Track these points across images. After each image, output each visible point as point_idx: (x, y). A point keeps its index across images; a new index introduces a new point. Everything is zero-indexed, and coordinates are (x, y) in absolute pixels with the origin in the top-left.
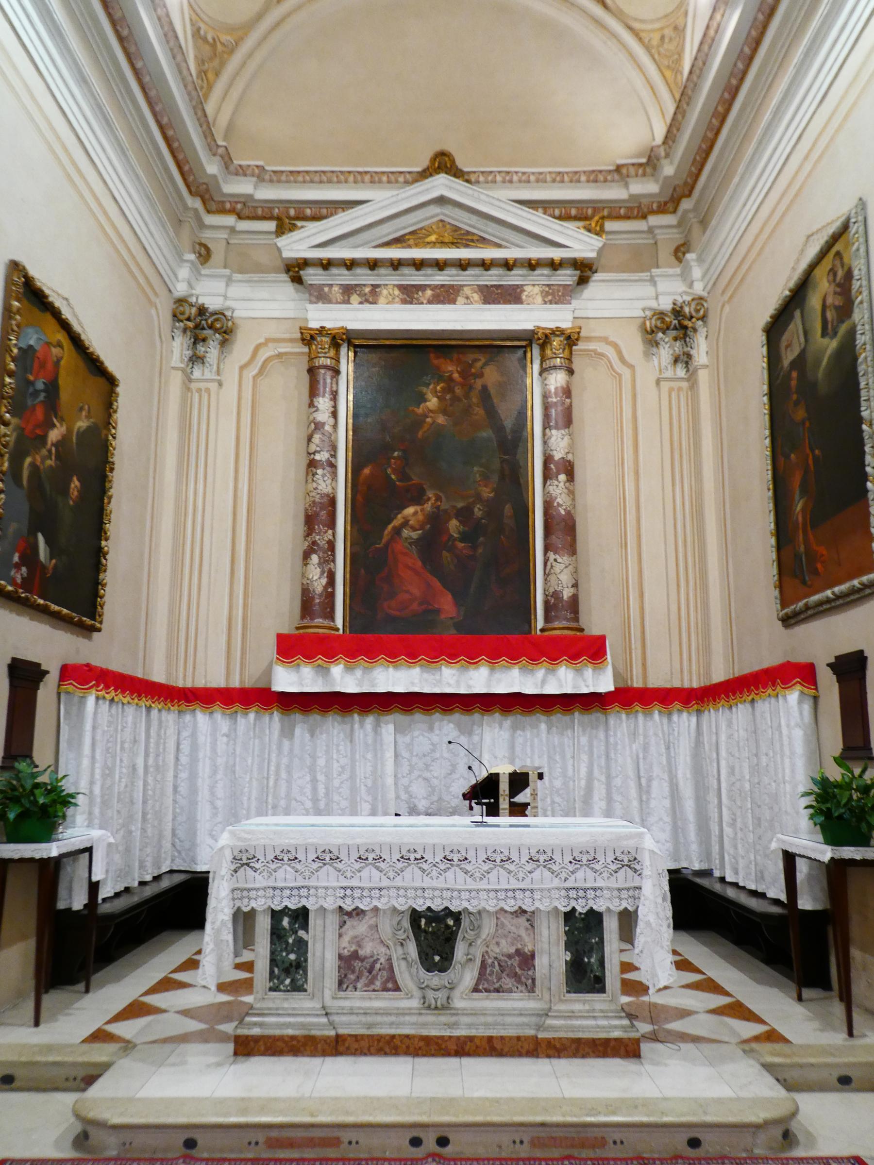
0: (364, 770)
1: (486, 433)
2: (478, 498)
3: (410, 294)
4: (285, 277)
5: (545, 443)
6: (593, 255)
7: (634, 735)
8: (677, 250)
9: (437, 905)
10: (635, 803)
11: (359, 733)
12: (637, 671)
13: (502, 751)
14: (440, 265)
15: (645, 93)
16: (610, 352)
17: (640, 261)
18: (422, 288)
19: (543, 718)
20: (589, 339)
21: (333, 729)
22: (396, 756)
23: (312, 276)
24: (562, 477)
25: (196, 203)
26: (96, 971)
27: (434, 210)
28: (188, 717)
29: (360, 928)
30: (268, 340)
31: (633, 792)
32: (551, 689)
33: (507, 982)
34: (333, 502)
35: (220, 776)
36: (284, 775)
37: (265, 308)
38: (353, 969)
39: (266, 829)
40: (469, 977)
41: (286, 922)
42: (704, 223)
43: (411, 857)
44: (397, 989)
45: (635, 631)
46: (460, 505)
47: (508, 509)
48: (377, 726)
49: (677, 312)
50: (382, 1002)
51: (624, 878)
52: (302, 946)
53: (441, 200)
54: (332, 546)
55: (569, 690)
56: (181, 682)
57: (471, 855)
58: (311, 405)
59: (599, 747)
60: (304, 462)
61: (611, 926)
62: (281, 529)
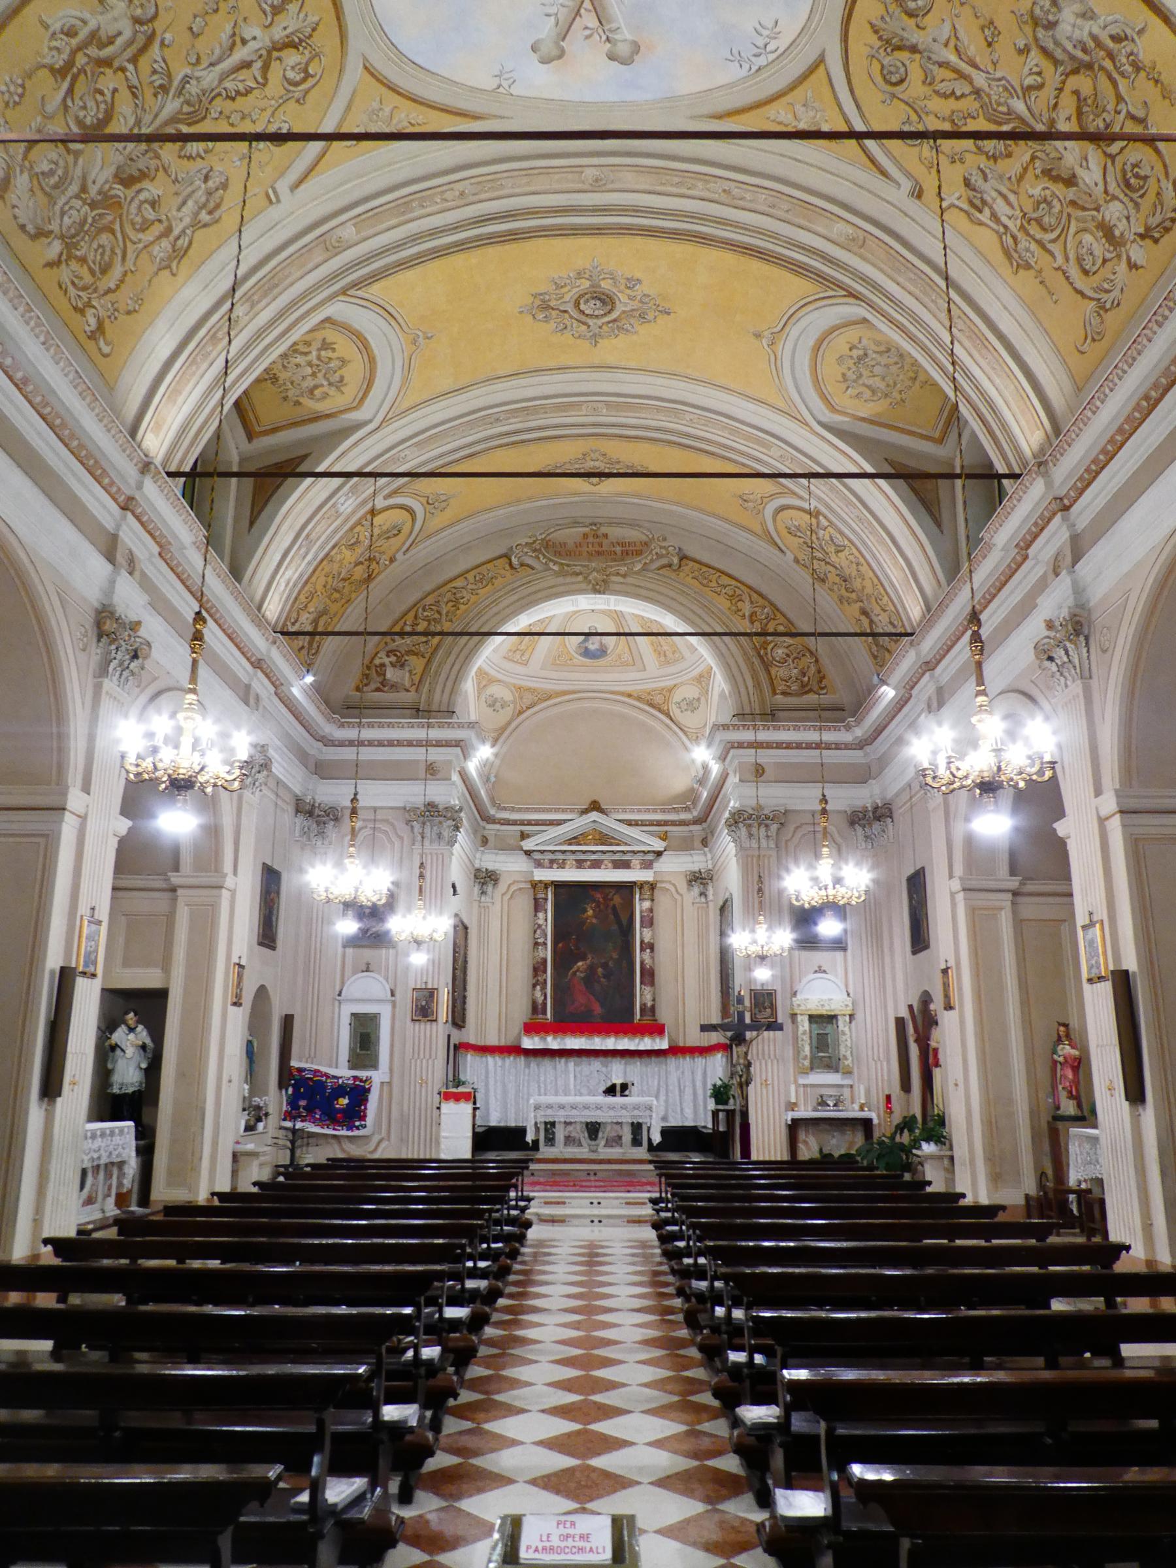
0: (560, 1082)
2: (611, 958)
3: (580, 864)
7: (677, 1068)
11: (558, 1066)
13: (621, 1075)
14: (594, 852)
16: (673, 889)
17: (685, 846)
20: (662, 882)
21: (547, 1063)
29: (570, 1128)
30: (514, 882)
31: (677, 1092)
32: (641, 1048)
34: (545, 960)
38: (569, 1140)
40: (603, 1143)
43: (586, 1107)
45: (681, 1021)
48: (566, 1063)
52: (554, 1133)
54: (545, 981)
55: (649, 1048)
56: (481, 1043)
59: (663, 1073)
60: (532, 942)
62: (521, 973)
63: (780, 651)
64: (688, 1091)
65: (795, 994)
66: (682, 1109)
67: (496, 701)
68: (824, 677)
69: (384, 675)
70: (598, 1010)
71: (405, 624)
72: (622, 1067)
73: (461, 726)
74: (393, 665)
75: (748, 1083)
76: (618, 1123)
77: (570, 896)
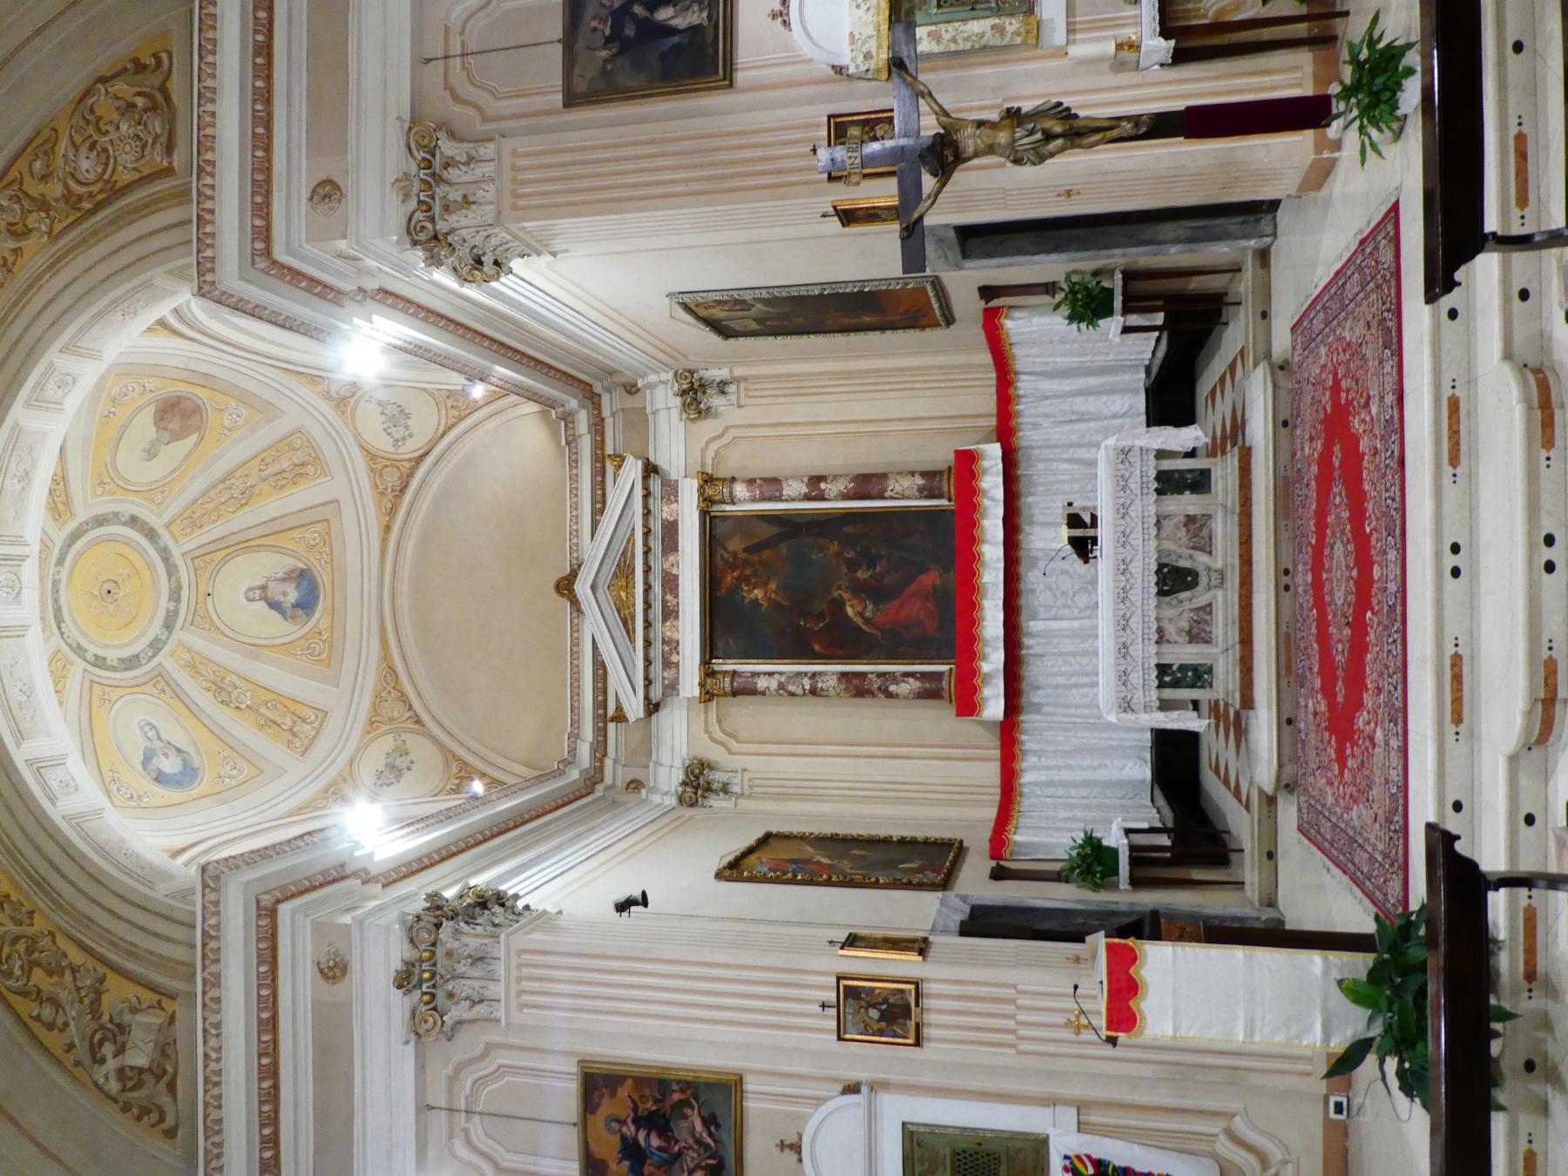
1: (784, 549)
2: (838, 554)
3: (670, 613)
4: (654, 717)
5: (793, 500)
6: (640, 463)
7: (1035, 426)
8: (630, 393)
9: (1154, 579)
10: (1092, 425)
12: (982, 422)
13: (1049, 533)
14: (648, 589)
15: (497, 421)
16: (715, 446)
17: (639, 423)
18: (664, 602)
19: (1023, 500)
20: (703, 464)
21: (1034, 671)
22: (1055, 619)
23: (656, 693)
24: (823, 485)
25: (600, 788)
26: (1214, 827)
27: (600, 592)
28: (1025, 790)
29: (1171, 630)
30: (707, 731)
31: (1083, 426)
33: (1205, 532)
34: (844, 675)
35: (1073, 763)
36: (1072, 711)
37: (680, 734)
38: (1198, 634)
39: (1106, 691)
40: (1202, 558)
41: (1167, 679)
42: (611, 372)
43: (1123, 596)
44: (1210, 605)
46: (844, 569)
47: (848, 529)
48: (1030, 635)
49: (683, 393)
50: (1219, 614)
51: (1134, 458)
52: (1183, 668)
53: (594, 588)
54: (881, 675)
55: (1000, 479)
56: (995, 795)
57: (1121, 557)
58: (763, 693)
59: (1047, 453)
60: (812, 698)
61: (1167, 465)
62: (868, 718)
63: (85, 164)
64: (1080, 404)
65: (839, 70)
66: (1114, 416)
67: (392, 767)
68: (136, 61)
69: (141, 1071)
70: (931, 578)
71: (38, 1019)
72: (1037, 530)
73: (214, 908)
74: (120, 1051)
75: (1066, 115)
76: (1158, 524)
77: (727, 626)
